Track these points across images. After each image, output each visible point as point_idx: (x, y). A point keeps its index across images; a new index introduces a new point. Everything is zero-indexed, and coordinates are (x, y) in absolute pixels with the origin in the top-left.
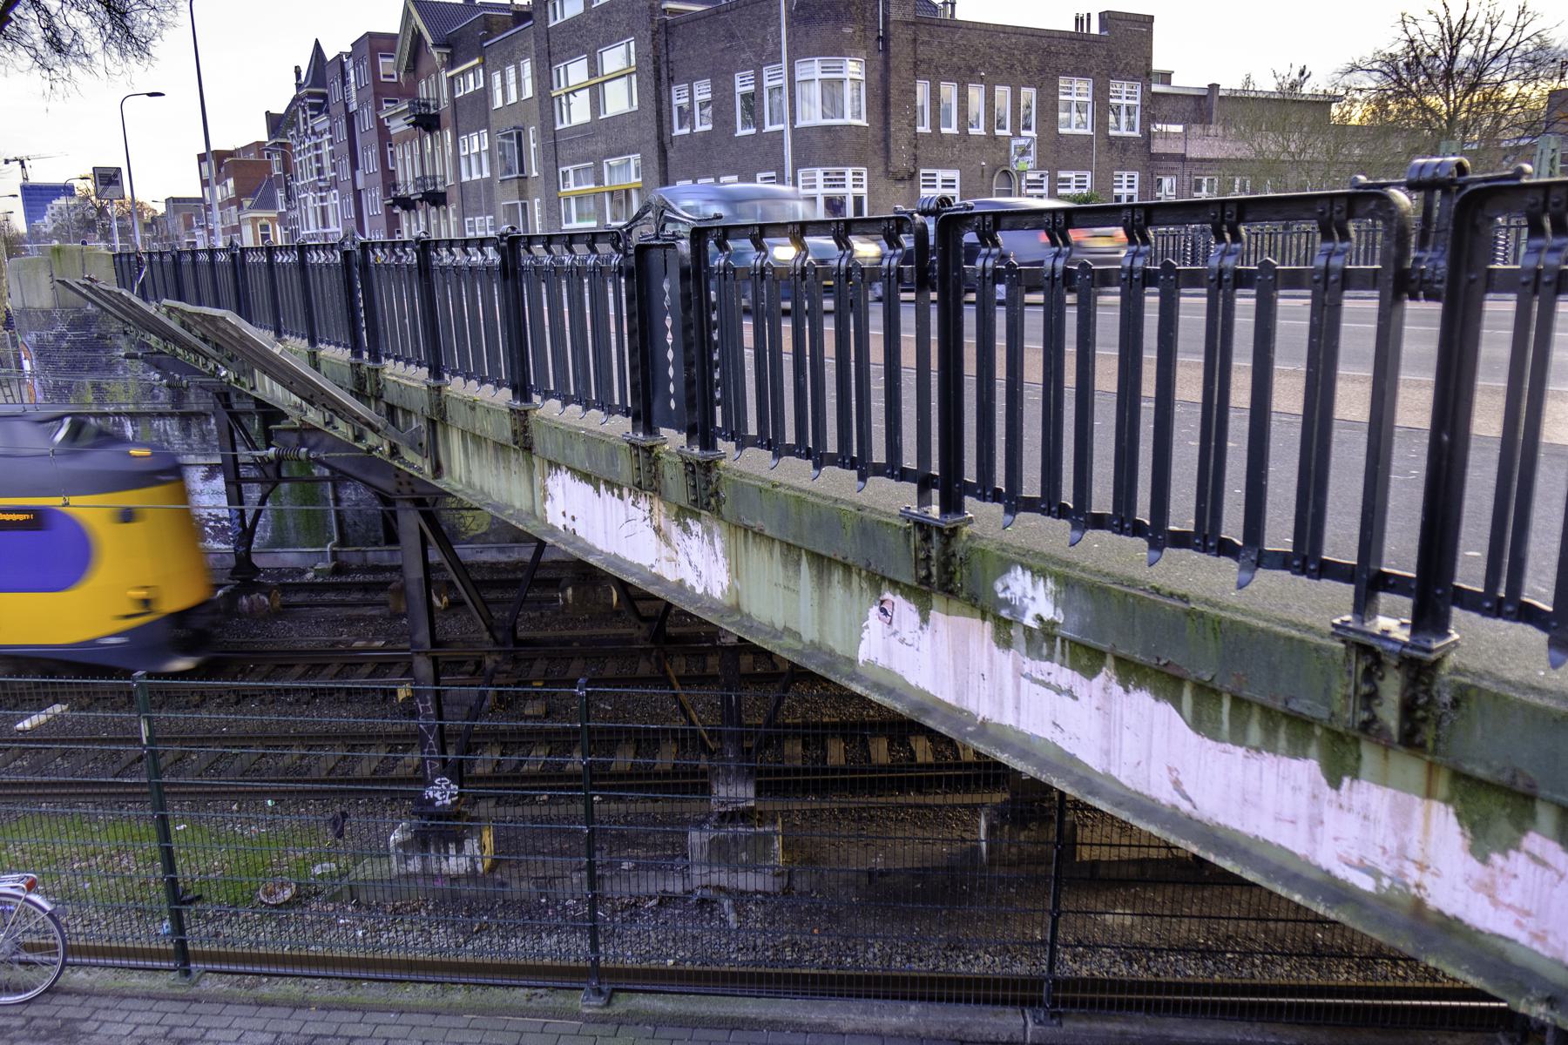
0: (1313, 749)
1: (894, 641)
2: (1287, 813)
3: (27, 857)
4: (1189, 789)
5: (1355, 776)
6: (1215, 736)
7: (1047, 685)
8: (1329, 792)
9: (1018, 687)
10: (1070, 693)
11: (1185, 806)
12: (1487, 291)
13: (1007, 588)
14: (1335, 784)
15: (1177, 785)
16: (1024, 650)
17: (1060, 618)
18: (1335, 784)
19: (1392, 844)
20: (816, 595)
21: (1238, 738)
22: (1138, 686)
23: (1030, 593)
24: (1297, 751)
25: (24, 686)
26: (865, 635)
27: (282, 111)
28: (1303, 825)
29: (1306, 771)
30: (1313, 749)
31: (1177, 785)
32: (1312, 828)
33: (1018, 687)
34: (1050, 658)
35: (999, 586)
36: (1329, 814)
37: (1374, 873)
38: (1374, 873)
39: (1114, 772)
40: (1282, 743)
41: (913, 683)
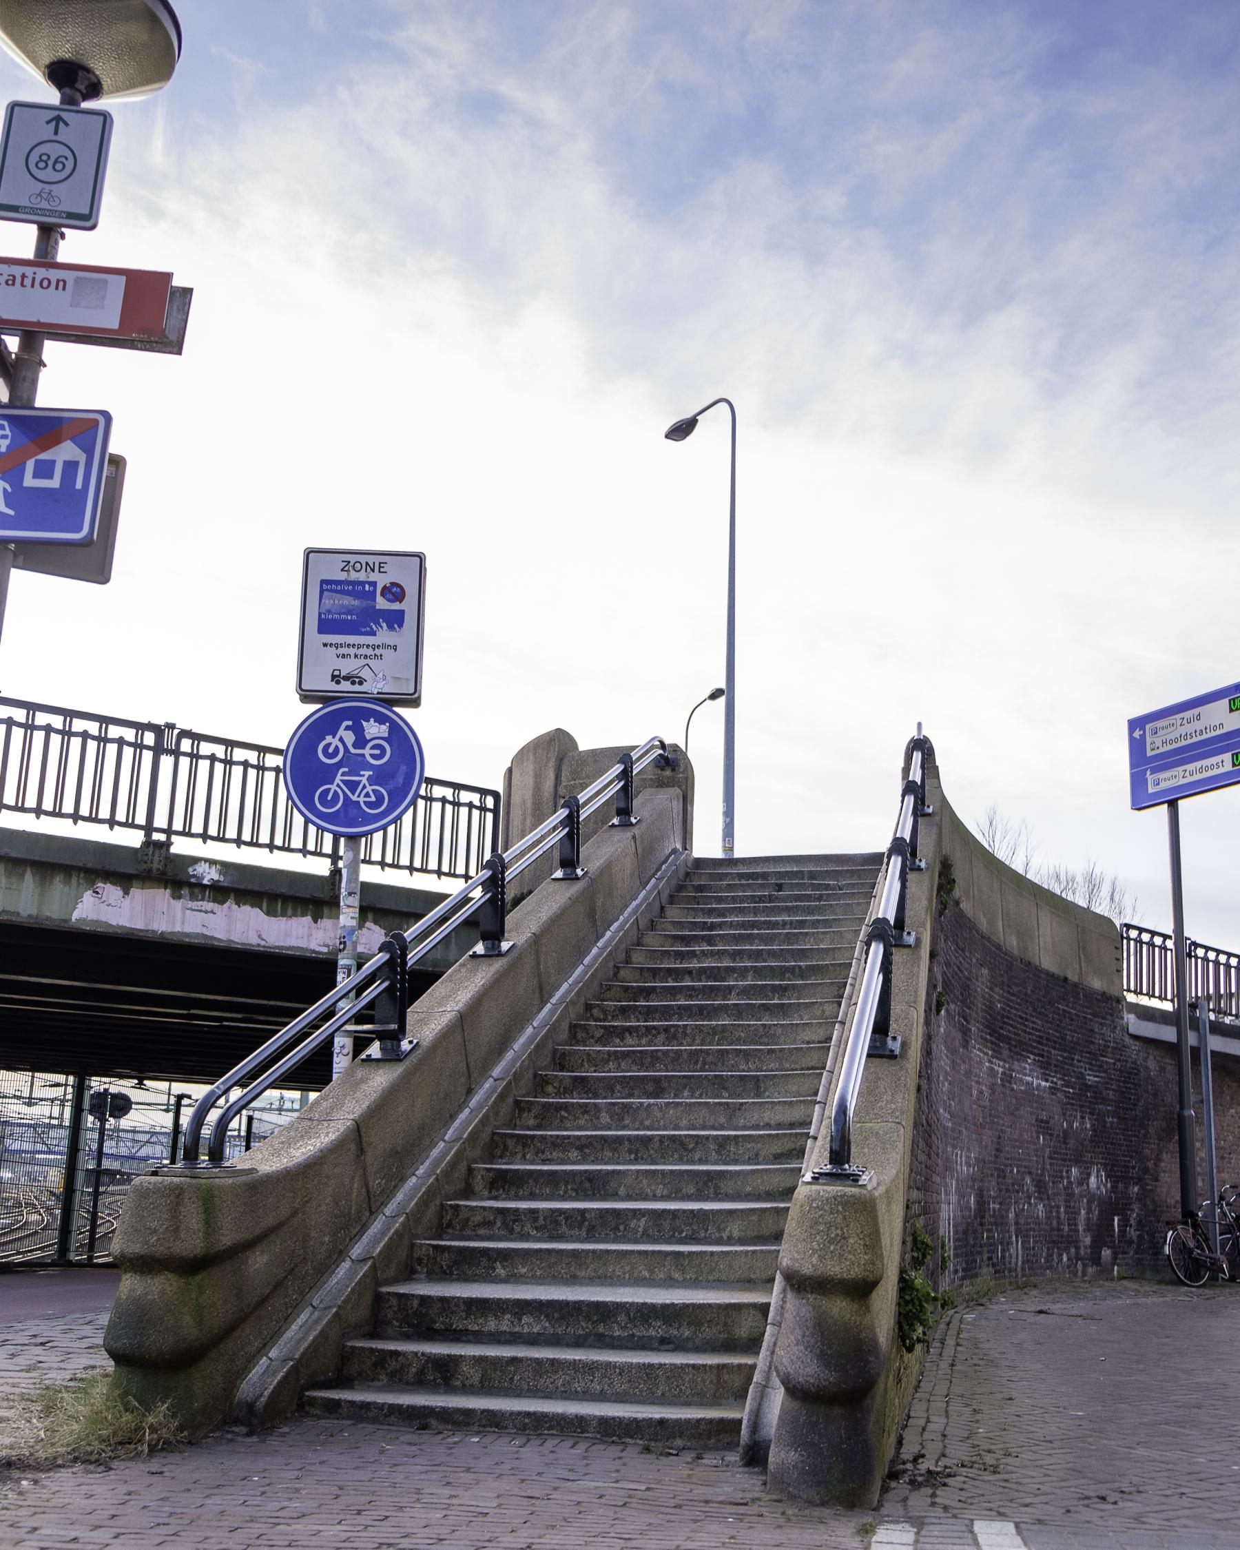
0: (309, 913)
1: (103, 906)
2: (300, 935)
3: (1022, 996)
4: (264, 937)
5: (322, 918)
6: (275, 916)
7: (201, 911)
8: (314, 925)
9: (184, 913)
10: (212, 912)
11: (263, 943)
12: (71, 440)
13: (195, 870)
14: (316, 922)
15: (260, 936)
16: (188, 898)
17: (222, 879)
18: (316, 922)
19: (332, 936)
20: (37, 891)
21: (284, 914)
22: (244, 904)
23: (207, 871)
24: (303, 915)
25: (670, 1067)
26: (80, 905)
27: (585, 744)
28: (305, 938)
29: (307, 920)
30: (309, 913)
31: (260, 936)
32: (309, 940)
33: (184, 913)
34: (203, 900)
35: (190, 870)
36: (314, 932)
37: (328, 946)
38: (328, 946)
39: (232, 938)
40: (290, 912)
41: (115, 924)
